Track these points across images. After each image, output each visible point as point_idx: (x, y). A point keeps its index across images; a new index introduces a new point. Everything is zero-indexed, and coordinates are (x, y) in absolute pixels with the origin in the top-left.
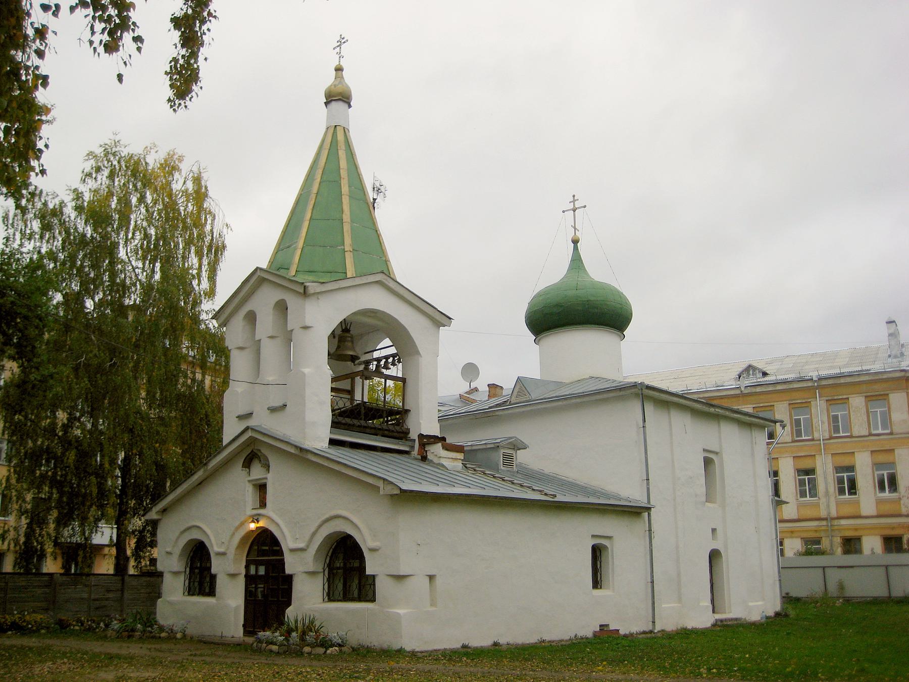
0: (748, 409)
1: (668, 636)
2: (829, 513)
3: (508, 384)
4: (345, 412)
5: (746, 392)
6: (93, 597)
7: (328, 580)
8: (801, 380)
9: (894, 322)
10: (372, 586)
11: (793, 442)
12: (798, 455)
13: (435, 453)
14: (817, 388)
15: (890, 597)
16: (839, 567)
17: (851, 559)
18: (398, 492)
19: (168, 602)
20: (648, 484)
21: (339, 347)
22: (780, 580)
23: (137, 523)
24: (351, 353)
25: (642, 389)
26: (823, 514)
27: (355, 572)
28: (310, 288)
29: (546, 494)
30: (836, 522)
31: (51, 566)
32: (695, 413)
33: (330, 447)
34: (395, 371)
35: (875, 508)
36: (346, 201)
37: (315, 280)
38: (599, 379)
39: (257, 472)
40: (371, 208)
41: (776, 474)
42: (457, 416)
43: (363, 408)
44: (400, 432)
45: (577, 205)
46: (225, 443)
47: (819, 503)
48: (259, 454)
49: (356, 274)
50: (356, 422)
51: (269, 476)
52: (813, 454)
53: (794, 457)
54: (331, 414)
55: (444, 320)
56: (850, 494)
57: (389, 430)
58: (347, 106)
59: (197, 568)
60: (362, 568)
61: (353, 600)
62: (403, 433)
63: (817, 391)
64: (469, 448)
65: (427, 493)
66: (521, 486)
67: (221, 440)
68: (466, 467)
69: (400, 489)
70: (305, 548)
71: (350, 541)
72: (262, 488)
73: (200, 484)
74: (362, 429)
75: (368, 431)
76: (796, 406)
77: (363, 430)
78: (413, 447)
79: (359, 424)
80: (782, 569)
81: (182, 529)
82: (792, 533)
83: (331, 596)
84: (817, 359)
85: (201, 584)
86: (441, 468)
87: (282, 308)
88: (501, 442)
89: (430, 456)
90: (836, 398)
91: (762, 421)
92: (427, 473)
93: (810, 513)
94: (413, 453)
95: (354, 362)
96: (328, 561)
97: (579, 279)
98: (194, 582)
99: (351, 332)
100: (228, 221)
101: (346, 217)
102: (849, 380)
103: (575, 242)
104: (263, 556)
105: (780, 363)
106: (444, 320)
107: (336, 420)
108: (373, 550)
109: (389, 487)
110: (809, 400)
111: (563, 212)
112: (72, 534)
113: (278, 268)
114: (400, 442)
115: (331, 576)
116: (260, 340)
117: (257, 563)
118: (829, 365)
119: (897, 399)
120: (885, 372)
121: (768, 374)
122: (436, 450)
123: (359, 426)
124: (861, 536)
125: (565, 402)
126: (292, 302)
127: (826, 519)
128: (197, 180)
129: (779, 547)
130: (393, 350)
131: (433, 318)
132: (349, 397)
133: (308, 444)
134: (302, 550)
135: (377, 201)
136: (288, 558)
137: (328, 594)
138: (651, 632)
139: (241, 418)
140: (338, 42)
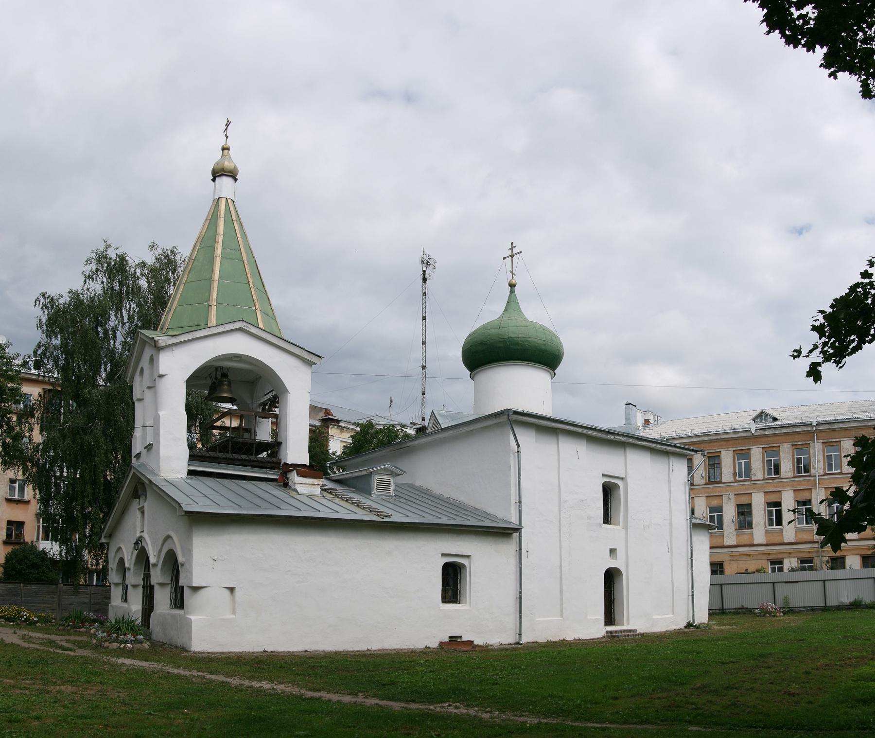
5: (757, 434)
6: (92, 592)
8: (803, 425)
11: (793, 477)
12: (798, 489)
14: (815, 431)
16: (786, 582)
17: (838, 573)
20: (520, 506)
45: (515, 251)
52: (810, 488)
53: (794, 490)
56: (807, 524)
63: (815, 434)
70: (156, 563)
76: (798, 447)
90: (830, 440)
102: (841, 426)
103: (512, 286)
111: (504, 259)
123: (224, 459)
124: (845, 556)
138: (518, 643)
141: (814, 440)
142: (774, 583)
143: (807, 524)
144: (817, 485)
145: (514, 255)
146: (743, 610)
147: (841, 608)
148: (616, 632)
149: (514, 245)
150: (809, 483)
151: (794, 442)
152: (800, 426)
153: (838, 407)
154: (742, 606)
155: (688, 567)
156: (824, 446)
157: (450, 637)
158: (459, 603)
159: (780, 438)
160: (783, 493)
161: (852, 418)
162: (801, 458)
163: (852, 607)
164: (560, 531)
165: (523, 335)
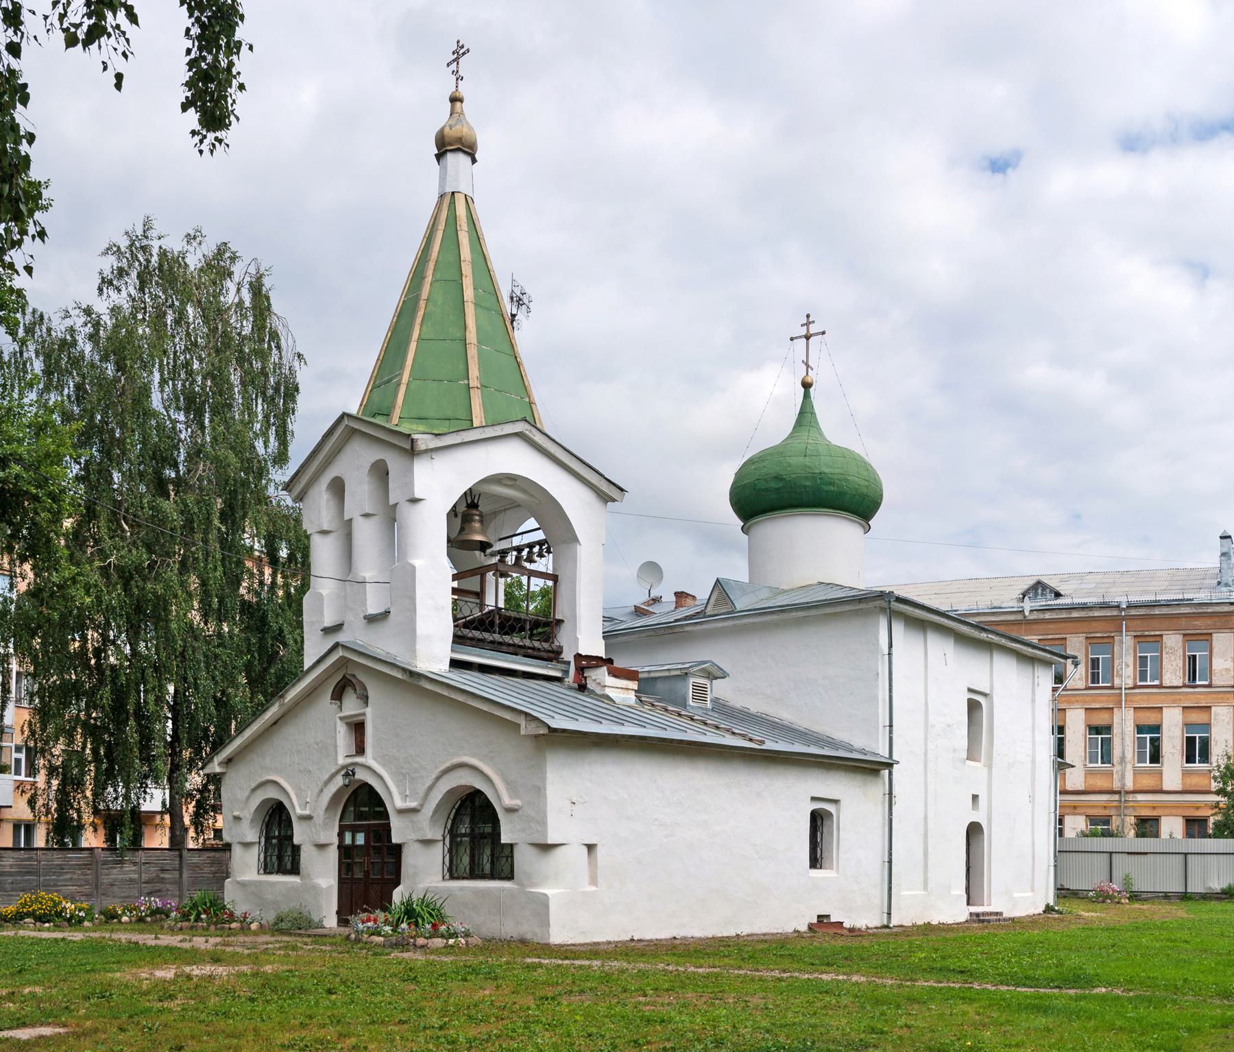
0: (1034, 639)
1: (905, 931)
2: (1123, 785)
3: (702, 591)
4: (471, 622)
5: (1031, 618)
7: (450, 851)
8: (1104, 606)
9: (1229, 537)
10: (509, 859)
13: (598, 681)
14: (1124, 618)
15: (1186, 893)
16: (1129, 853)
17: (1146, 844)
18: (543, 731)
19: (238, 882)
20: (891, 732)
21: (462, 529)
22: (1055, 866)
23: (195, 780)
24: (479, 538)
25: (890, 601)
26: (1116, 785)
27: (486, 841)
28: (419, 443)
29: (751, 740)
30: (1131, 797)
31: (92, 839)
32: (962, 639)
33: (452, 670)
34: (544, 564)
35: (1180, 782)
36: (470, 310)
37: (426, 431)
38: (831, 586)
39: (351, 706)
40: (509, 327)
41: (1061, 730)
42: (632, 632)
43: (497, 617)
44: (549, 651)
45: (813, 329)
46: (306, 666)
47: (1113, 771)
48: (354, 681)
49: (486, 423)
50: (486, 635)
51: (368, 711)
52: (1111, 706)
53: (1086, 709)
54: (451, 624)
55: (613, 493)
56: (1103, 762)
57: (533, 648)
58: (468, 160)
59: (274, 837)
60: (496, 834)
61: (483, 877)
62: (553, 652)
64: (645, 675)
65: (586, 733)
66: (717, 728)
67: (302, 662)
68: (641, 701)
69: (549, 727)
70: (418, 808)
71: (480, 798)
72: (358, 728)
73: (275, 723)
74: (496, 645)
75: (504, 648)
76: (1095, 641)
77: (497, 647)
78: (566, 672)
79: (491, 638)
80: (1059, 853)
81: (254, 785)
82: (1075, 809)
83: (453, 873)
84: (1128, 580)
85: (280, 858)
86: (606, 701)
87: (380, 472)
88: (691, 667)
89: (590, 685)
90: (1147, 633)
91: (1049, 656)
92: (586, 707)
93: (1101, 783)
94: (566, 680)
95: (484, 552)
96: (449, 826)
97: (810, 441)
98: (271, 856)
99: (479, 508)
100: (300, 349)
101: (472, 336)
102: (1165, 611)
103: (807, 386)
104: (362, 820)
105: (1080, 582)
106: (613, 493)
107: (459, 633)
108: (510, 810)
109: (533, 724)
110: (1113, 635)
111: (792, 339)
112: (115, 799)
113: (374, 411)
114: (550, 665)
115: (454, 844)
116: (351, 520)
117: (354, 830)
118: (1142, 588)
119: (1221, 640)
120: (1211, 604)
121: (1062, 596)
122: (600, 677)
123: (492, 642)
125: (782, 616)
126: (394, 463)
127: (1119, 792)
128: (257, 289)
129: (1058, 826)
130: (540, 536)
131: (598, 489)
132: (478, 601)
133: (422, 666)
134: (414, 811)
135: (517, 318)
136: (395, 822)
137: (450, 870)
138: (887, 927)
139: (327, 631)
140: (454, 53)
141: (1122, 632)
142: (1111, 853)
143: (1103, 762)
144: (1123, 702)
145: (811, 335)
146: (1062, 892)
147: (1206, 897)
148: (983, 914)
149: (811, 320)
150: (1111, 698)
151: (1090, 633)
152: (1101, 607)
153: (1151, 579)
154: (1062, 885)
155: (1049, 824)
156: (1136, 641)
157: (819, 917)
158: (821, 868)
159: (1068, 625)
160: (1068, 713)
161: (1182, 600)
162: (1098, 658)
163: (1223, 896)
164: (925, 768)
165: (839, 471)
